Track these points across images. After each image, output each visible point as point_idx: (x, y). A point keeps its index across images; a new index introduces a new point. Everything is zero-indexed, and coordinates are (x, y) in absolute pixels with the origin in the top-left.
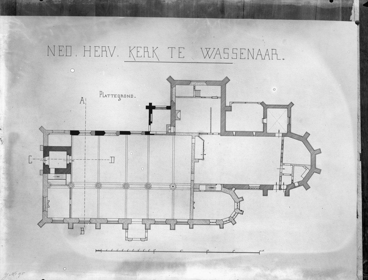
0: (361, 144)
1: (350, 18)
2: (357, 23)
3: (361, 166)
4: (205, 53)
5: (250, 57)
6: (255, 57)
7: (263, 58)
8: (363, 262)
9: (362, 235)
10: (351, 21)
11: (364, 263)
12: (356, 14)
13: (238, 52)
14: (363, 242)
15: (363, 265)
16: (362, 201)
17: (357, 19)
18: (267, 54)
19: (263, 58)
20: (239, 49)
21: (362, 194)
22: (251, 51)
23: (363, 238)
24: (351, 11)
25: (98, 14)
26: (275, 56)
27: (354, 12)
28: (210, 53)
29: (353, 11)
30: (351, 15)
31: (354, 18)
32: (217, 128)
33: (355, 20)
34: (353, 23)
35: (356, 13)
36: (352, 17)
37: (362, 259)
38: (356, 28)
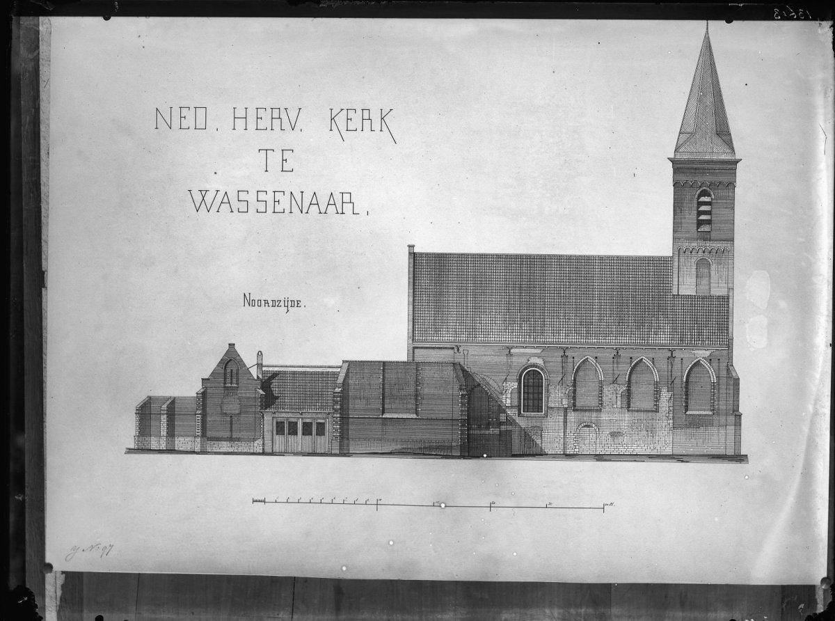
0: (42, 307)
1: (66, 578)
2: (49, 567)
3: (43, 260)
4: (198, 198)
5: (295, 209)
6: (305, 211)
7: (323, 211)
8: (39, 54)
9: (41, 112)
10: (63, 572)
11: (37, 52)
12: (52, 588)
13: (269, 198)
14: (38, 96)
15: (39, 47)
16: (40, 184)
17: (49, 577)
18: (332, 202)
19: (323, 211)
20: (271, 194)
21: (40, 201)
22: (298, 196)
23: (39, 105)
24: (62, 594)
25: (608, 587)
26: (348, 208)
27: (56, 592)
28: (209, 198)
29: (59, 593)
30: (62, 586)
31: (57, 579)
32: (417, 345)
33: (53, 574)
34: (58, 567)
35: (53, 590)
36: (61, 580)
37: (41, 60)
38: (49, 558)
